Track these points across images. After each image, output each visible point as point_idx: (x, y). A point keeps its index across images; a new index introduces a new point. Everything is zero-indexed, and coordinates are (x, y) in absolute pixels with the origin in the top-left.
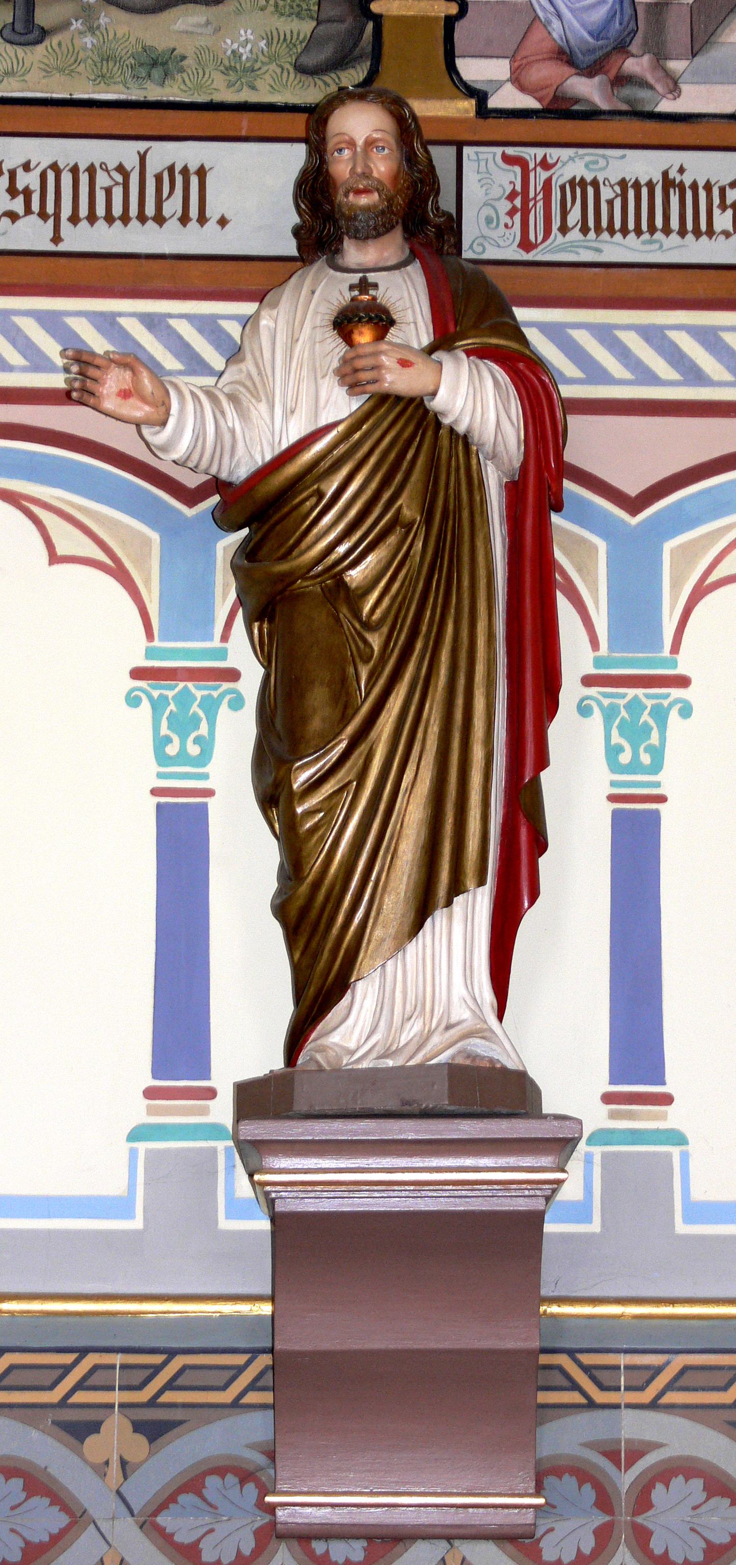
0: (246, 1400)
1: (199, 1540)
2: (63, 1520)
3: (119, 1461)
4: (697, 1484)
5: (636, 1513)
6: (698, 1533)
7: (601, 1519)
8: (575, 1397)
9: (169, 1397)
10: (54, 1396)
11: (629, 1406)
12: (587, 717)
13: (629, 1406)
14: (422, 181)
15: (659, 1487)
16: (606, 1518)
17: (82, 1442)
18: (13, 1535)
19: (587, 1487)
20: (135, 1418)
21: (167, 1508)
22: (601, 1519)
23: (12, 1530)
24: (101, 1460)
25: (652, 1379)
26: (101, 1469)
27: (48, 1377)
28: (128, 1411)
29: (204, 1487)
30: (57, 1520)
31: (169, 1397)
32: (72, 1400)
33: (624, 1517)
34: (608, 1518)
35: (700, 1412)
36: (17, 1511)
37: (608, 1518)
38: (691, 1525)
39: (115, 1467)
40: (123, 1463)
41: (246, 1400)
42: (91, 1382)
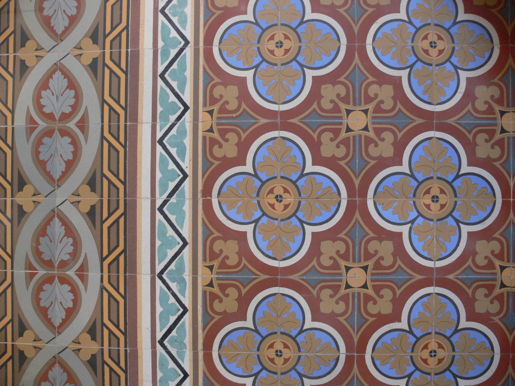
0: (105, 105)
1: (49, 381)
2: (59, 32)
3: (80, 348)
4: (71, 305)
5: (60, 130)
6: (51, 305)
7: (57, 133)
8: (105, 253)
9: (107, 71)
10: (106, 321)
11: (13, 124)
12: (336, 251)
13: (13, 124)
14: (491, 133)
15: (69, 288)
16: (57, 117)
17: (87, 184)
18: (50, 303)
19: (44, 287)
20: (96, 206)
21: (61, 368)
22: (57, 133)
23: (52, 302)
24: (81, 340)
25: (115, 63)
26: (76, 342)
27: (115, 95)
28: (102, 56)
29: (70, 384)
30: (57, 322)
31: (107, 71)
32: (104, 179)
33: (57, 125)
34: (57, 119)
35: (100, 152)
36: (60, 304)
37: (57, 119)
38: (53, 154)
39: (77, 346)
40: (79, 350)
41: (105, 105)
42: (113, 76)
